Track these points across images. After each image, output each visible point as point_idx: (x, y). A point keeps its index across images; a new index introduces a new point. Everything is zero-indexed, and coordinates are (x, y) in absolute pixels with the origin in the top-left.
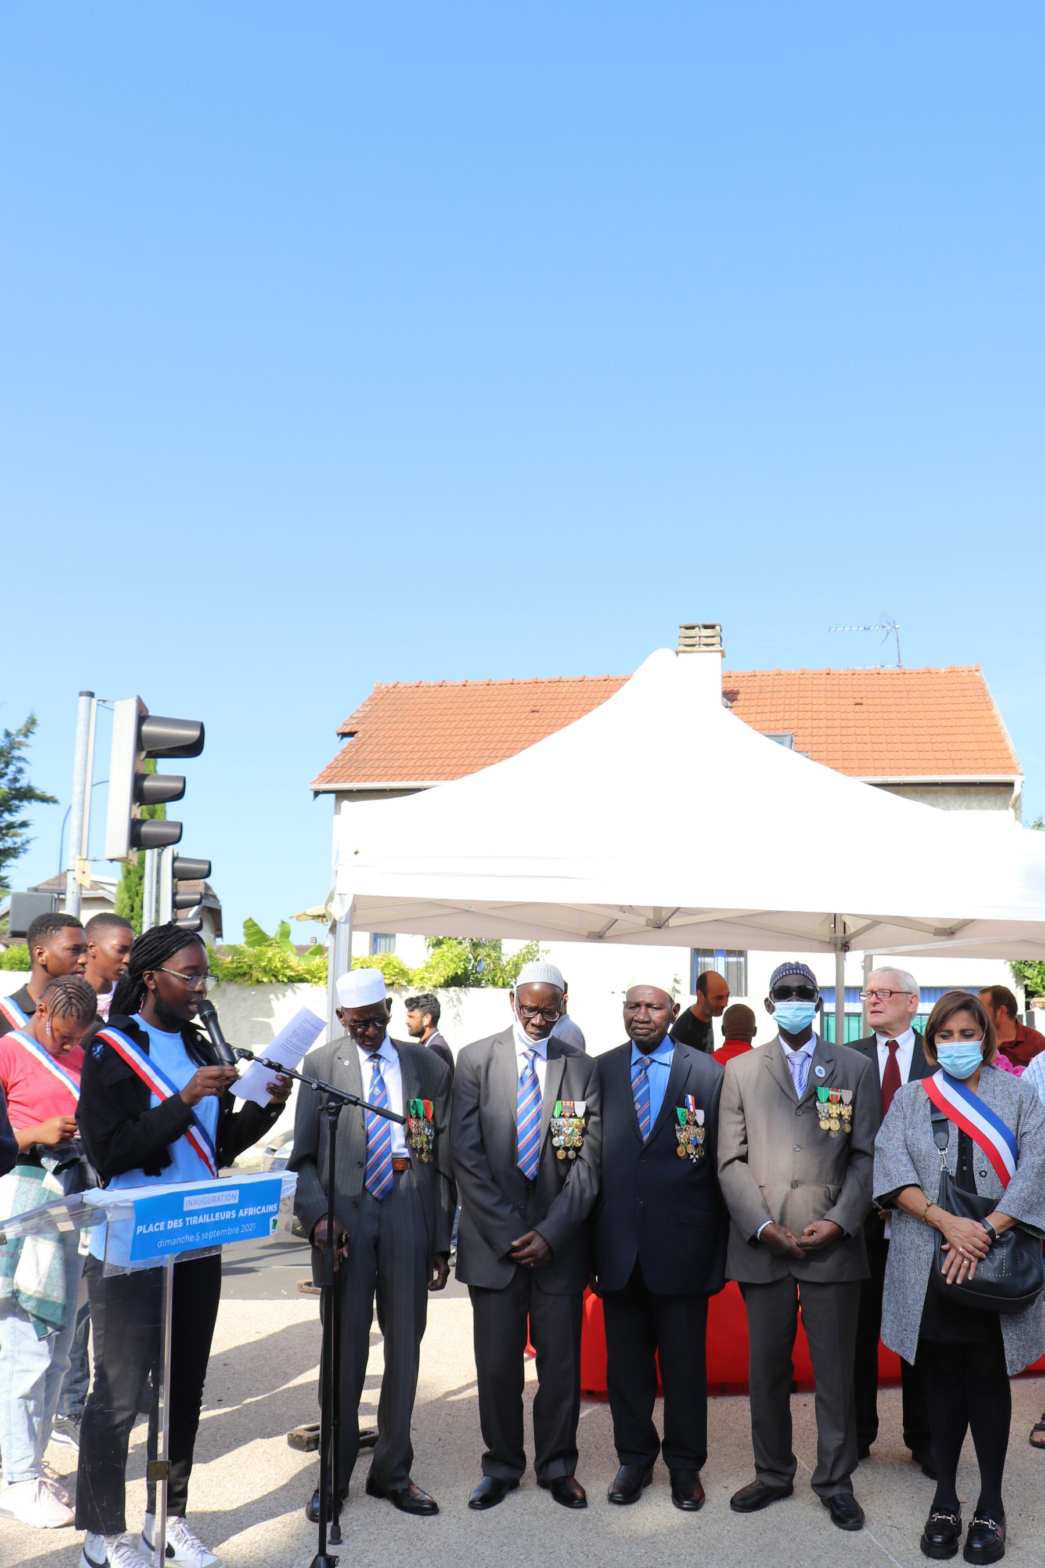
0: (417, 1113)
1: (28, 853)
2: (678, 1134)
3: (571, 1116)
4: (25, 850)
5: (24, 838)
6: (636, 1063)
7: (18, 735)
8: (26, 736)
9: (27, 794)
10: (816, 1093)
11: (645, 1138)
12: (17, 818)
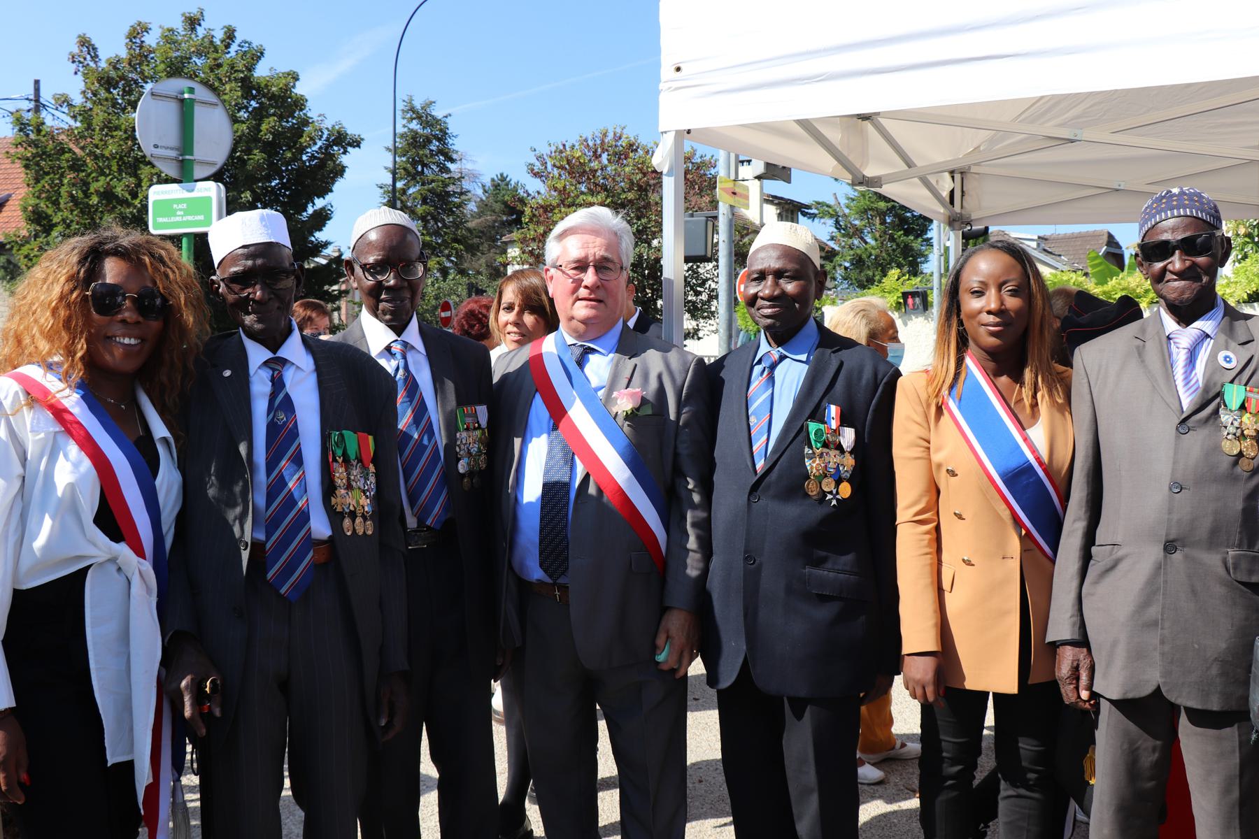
0: (345, 454)
2: (808, 462)
3: (475, 429)
10: (1220, 394)
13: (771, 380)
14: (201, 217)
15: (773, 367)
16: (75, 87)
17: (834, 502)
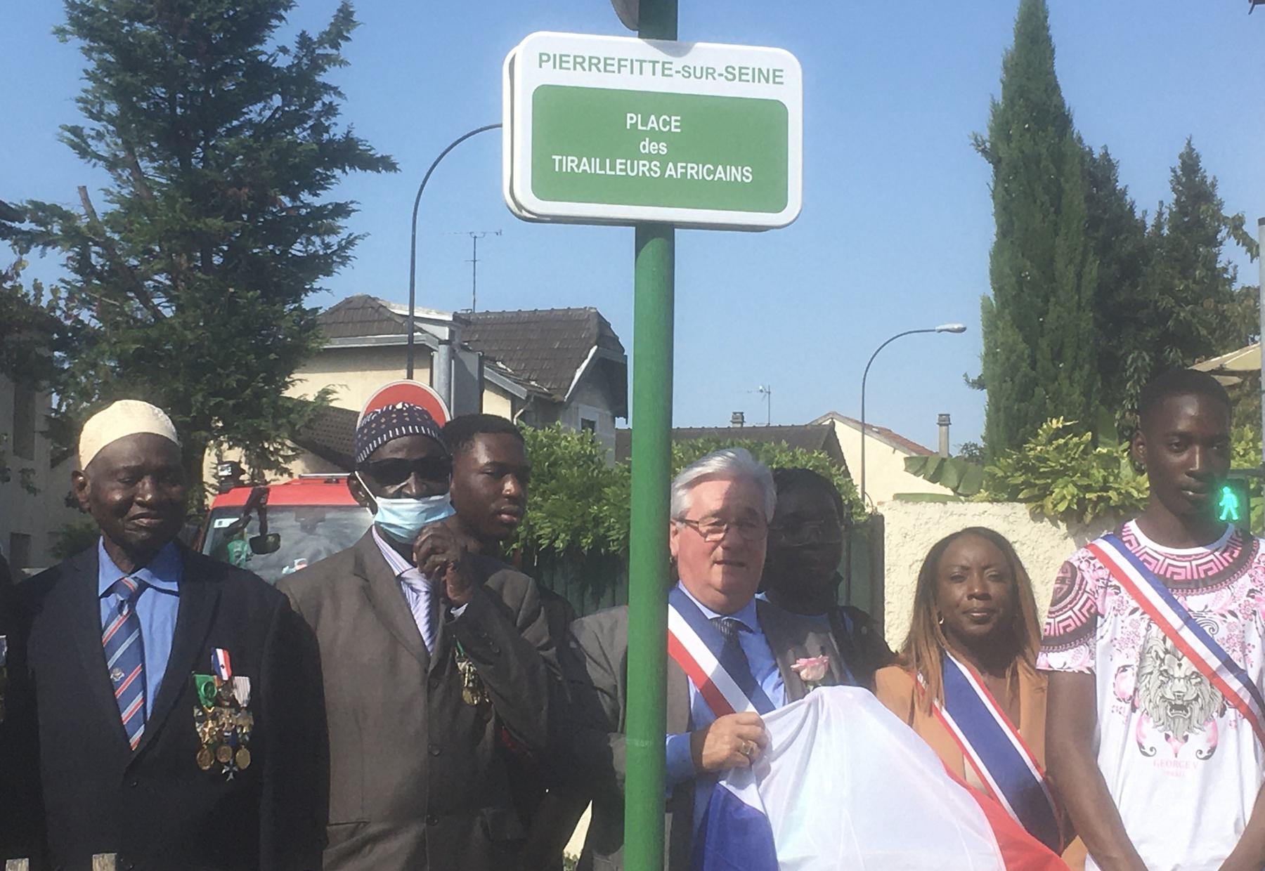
1: (354, 262)
4: (345, 260)
5: (344, 234)
6: (107, 593)
7: (321, 43)
8: (336, 46)
9: (350, 154)
11: (135, 738)
12: (325, 198)
13: (133, 622)
14: (742, 174)
15: (133, 598)
16: (90, 85)
17: (231, 776)
